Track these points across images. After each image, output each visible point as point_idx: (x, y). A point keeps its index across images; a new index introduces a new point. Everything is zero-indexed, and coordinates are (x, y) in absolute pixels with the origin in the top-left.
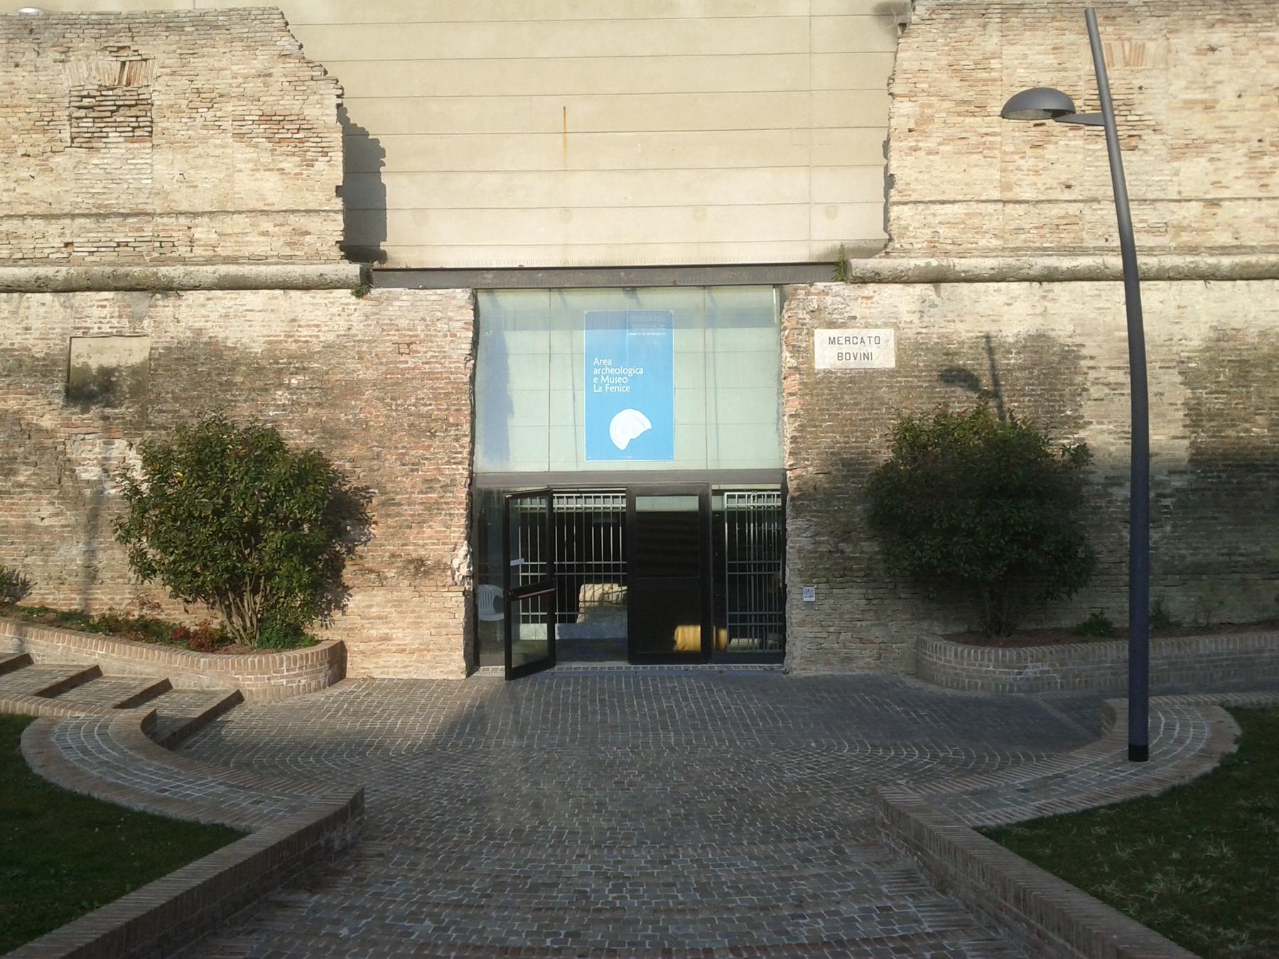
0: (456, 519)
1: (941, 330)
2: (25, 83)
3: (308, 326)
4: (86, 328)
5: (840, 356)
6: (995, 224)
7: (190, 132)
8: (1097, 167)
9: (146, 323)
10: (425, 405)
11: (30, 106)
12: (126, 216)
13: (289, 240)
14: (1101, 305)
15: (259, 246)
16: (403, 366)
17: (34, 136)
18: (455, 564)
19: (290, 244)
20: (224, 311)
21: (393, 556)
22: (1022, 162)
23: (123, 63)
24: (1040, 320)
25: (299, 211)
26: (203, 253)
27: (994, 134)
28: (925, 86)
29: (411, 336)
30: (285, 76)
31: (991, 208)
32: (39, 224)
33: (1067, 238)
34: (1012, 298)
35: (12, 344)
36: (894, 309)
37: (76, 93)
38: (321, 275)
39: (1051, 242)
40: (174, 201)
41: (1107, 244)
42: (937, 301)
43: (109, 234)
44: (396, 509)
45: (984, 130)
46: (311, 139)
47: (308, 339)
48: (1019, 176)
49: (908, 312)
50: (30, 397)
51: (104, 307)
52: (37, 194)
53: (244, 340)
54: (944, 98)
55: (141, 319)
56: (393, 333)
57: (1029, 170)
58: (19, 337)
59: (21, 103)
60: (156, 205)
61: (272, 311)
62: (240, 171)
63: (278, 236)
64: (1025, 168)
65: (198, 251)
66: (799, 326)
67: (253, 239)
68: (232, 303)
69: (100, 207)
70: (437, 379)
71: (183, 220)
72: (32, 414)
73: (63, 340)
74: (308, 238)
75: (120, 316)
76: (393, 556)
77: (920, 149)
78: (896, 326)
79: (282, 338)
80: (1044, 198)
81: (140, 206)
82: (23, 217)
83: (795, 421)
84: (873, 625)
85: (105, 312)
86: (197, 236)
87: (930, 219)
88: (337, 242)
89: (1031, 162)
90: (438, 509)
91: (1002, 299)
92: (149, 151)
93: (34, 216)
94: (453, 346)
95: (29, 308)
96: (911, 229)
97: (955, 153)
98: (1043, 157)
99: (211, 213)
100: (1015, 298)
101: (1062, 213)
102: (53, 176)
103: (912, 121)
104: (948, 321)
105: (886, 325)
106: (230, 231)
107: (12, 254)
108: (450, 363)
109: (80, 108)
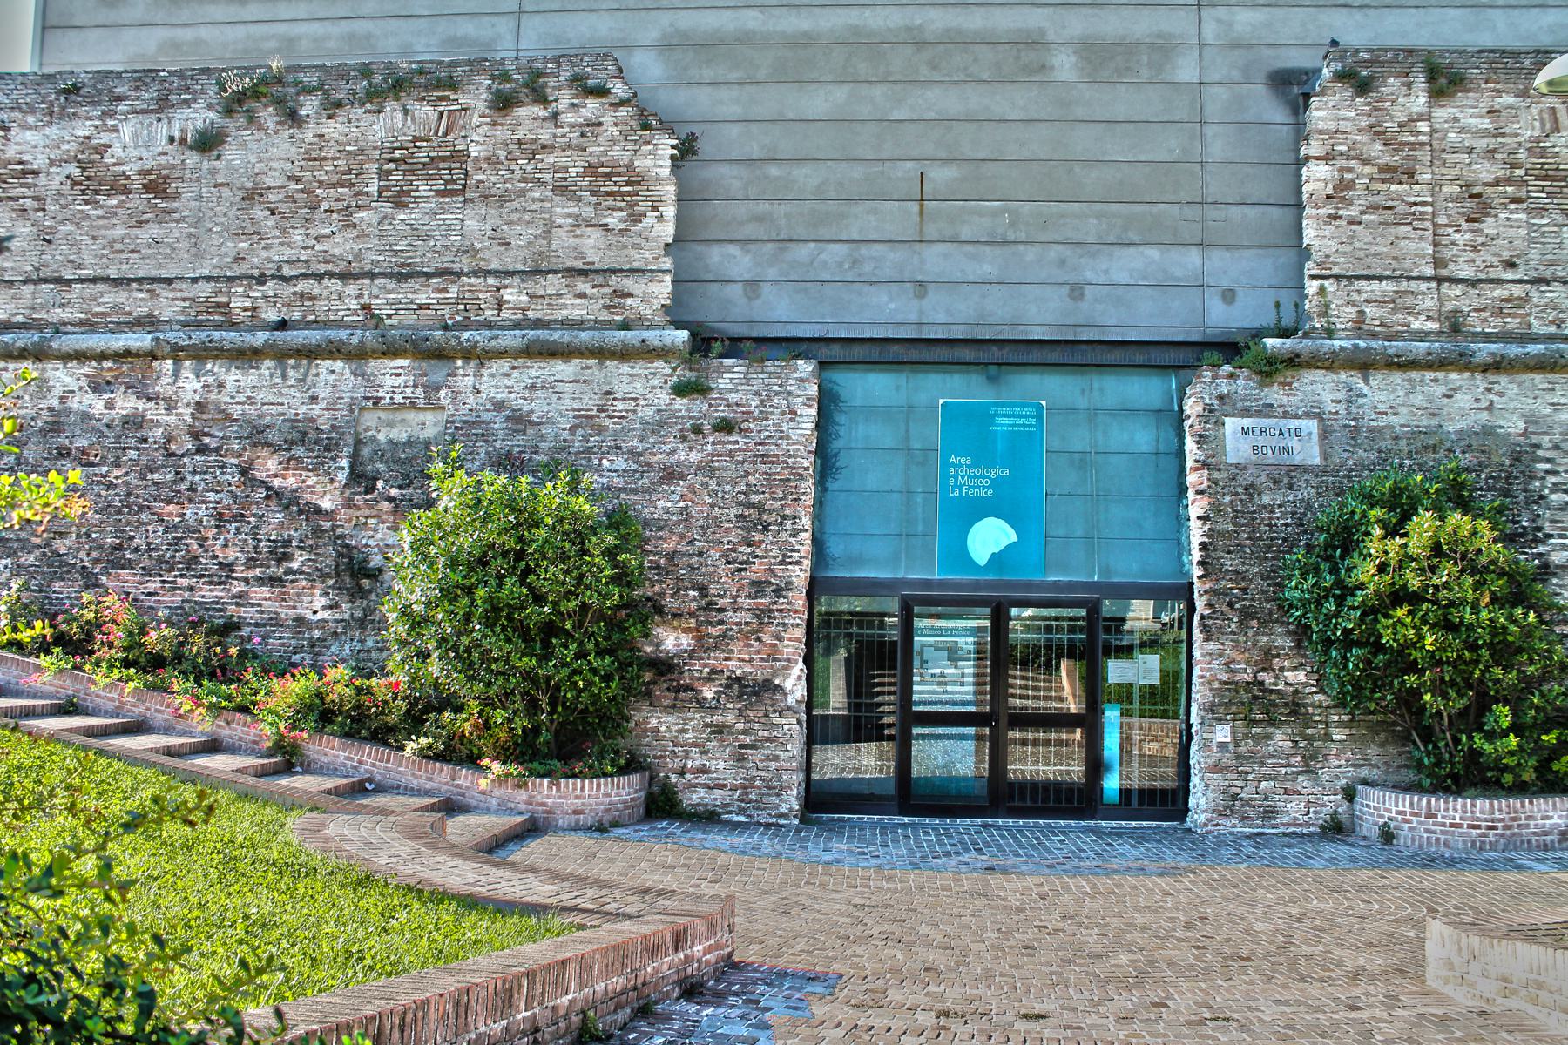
0: (790, 630)
1: (1372, 423)
2: (336, 135)
3: (624, 399)
4: (377, 398)
5: (1255, 449)
6: (1428, 304)
7: (507, 185)
8: (1544, 244)
9: (442, 393)
10: (757, 493)
11: (339, 158)
12: (429, 276)
14: (1555, 400)
15: (574, 309)
16: (731, 447)
17: (339, 190)
18: (788, 685)
21: (713, 671)
22: (1457, 236)
23: (441, 114)
24: (1485, 415)
25: (622, 271)
26: (513, 317)
27: (1424, 204)
28: (1344, 148)
29: (744, 413)
30: (616, 124)
31: (1423, 286)
32: (336, 284)
33: (1512, 323)
34: (1451, 389)
35: (297, 414)
36: (1317, 397)
37: (388, 145)
38: (643, 341)
39: (1494, 327)
40: (483, 259)
41: (1559, 332)
42: (1366, 390)
43: (410, 296)
44: (721, 616)
45: (1412, 199)
48: (1455, 252)
49: (1333, 401)
50: (310, 474)
51: (399, 375)
52: (337, 251)
53: (551, 414)
54: (1365, 162)
55: (438, 389)
57: (1465, 245)
58: (305, 407)
59: (330, 155)
60: (464, 264)
61: (585, 382)
62: (559, 226)
63: (597, 299)
64: (1461, 243)
65: (505, 314)
66: (1206, 413)
69: (403, 265)
70: (773, 463)
71: (491, 281)
72: (312, 493)
73: (352, 411)
74: (629, 301)
75: (415, 386)
76: (713, 671)
77: (1340, 217)
78: (1319, 417)
79: (594, 413)
80: (1483, 276)
81: (446, 265)
82: (319, 277)
83: (1205, 524)
84: (1301, 773)
85: (399, 381)
86: (506, 298)
87: (1355, 296)
88: (663, 306)
89: (1468, 236)
90: (769, 617)
91: (1439, 390)
92: (459, 205)
93: (331, 275)
94: (792, 425)
95: (317, 375)
96: (1333, 306)
97: (1380, 223)
98: (1481, 231)
99: (523, 272)
100: (1455, 390)
101: (1506, 294)
102: (355, 233)
103: (1330, 186)
104: (1380, 413)
105: (1307, 415)
106: (542, 293)
107: (304, 317)
108: (788, 444)
109: (391, 161)
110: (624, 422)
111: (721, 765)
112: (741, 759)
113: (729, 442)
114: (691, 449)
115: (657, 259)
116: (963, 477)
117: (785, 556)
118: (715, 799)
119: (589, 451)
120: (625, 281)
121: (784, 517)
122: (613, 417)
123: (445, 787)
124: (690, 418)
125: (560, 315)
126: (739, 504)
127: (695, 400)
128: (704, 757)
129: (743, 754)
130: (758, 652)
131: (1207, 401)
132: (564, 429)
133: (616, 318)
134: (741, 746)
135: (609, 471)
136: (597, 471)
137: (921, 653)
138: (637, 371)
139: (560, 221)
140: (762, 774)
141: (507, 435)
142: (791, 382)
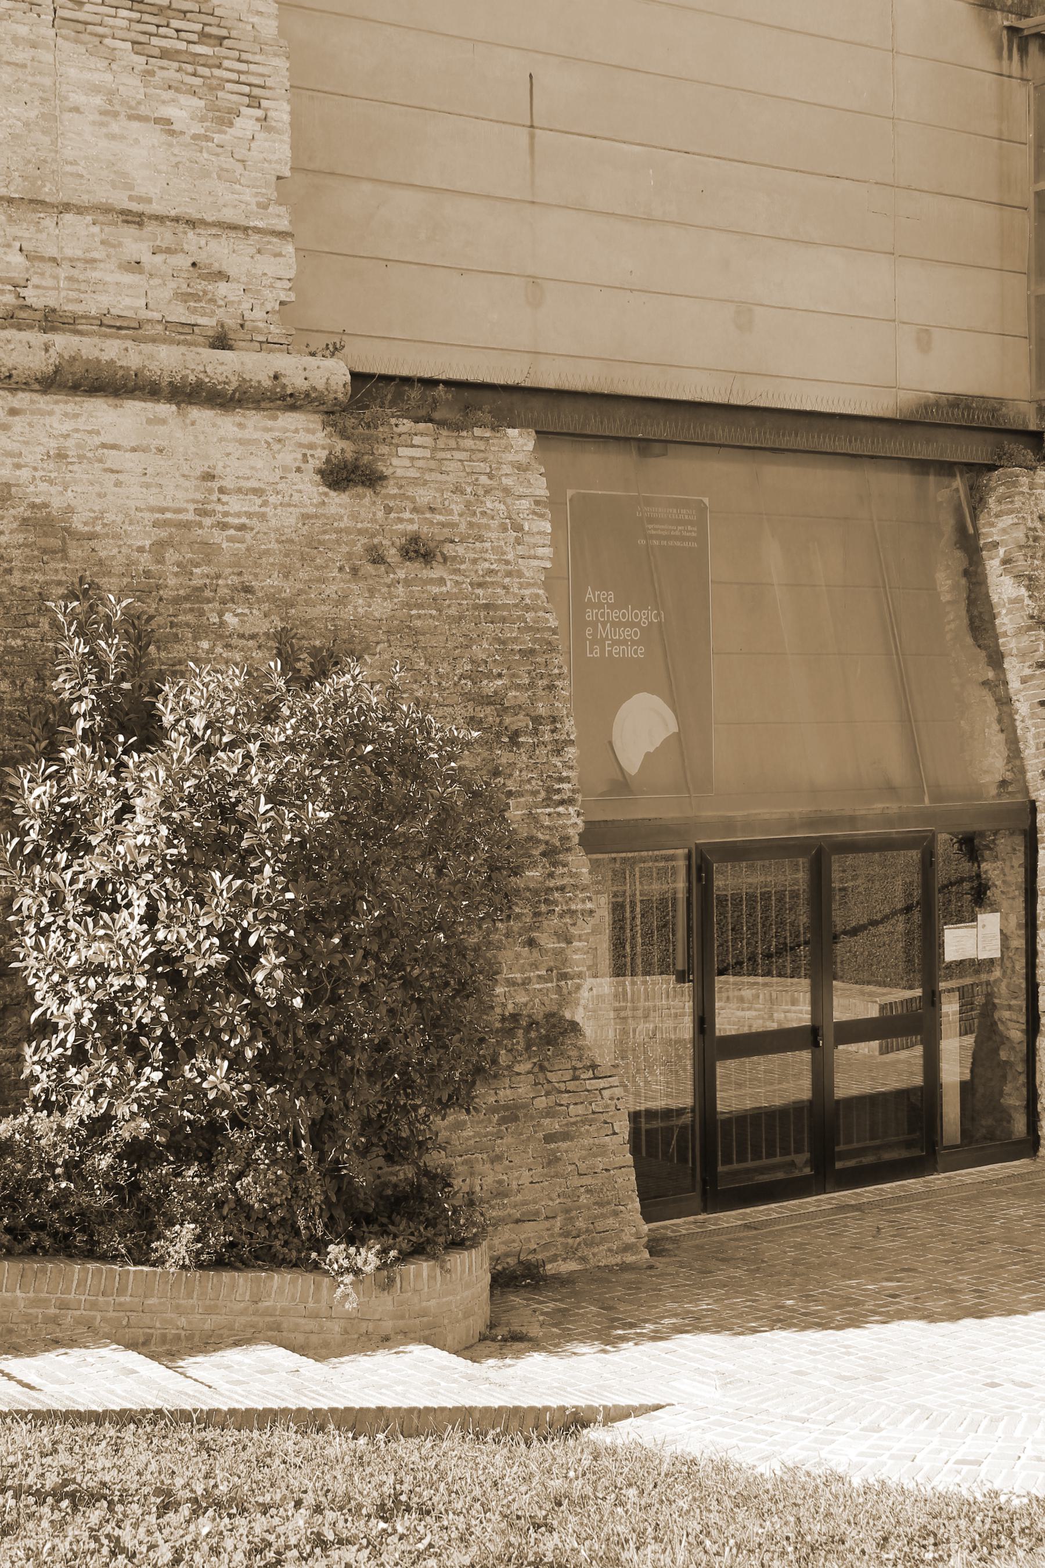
3: (239, 490)
10: (490, 676)
13: (184, 288)
16: (435, 590)
19: (185, 297)
20: (53, 444)
25: (204, 223)
29: (443, 525)
46: (226, 63)
47: (244, 520)
53: (109, 517)
56: (407, 515)
62: (76, 110)
67: (109, 278)
68: (67, 426)
70: (504, 620)
74: (222, 289)
94: (521, 550)
106: (52, 251)
108: (521, 586)
110: (248, 536)
111: (526, 1176)
112: (553, 1160)
113: (431, 581)
114: (372, 592)
115: (265, 207)
117: (550, 791)
118: (528, 1240)
119: (196, 595)
120: (213, 244)
121: (537, 720)
122: (224, 526)
123: (243, 1320)
124: (360, 532)
125: (93, 306)
126: (467, 697)
127: (361, 497)
128: (498, 1167)
129: (553, 1152)
130: (535, 966)
131: (1030, 524)
132: (141, 550)
133: (201, 321)
134: (549, 1138)
135: (242, 636)
136: (221, 637)
138: (249, 433)
139: (78, 98)
140: (586, 1180)
141: (30, 559)
142: (506, 469)
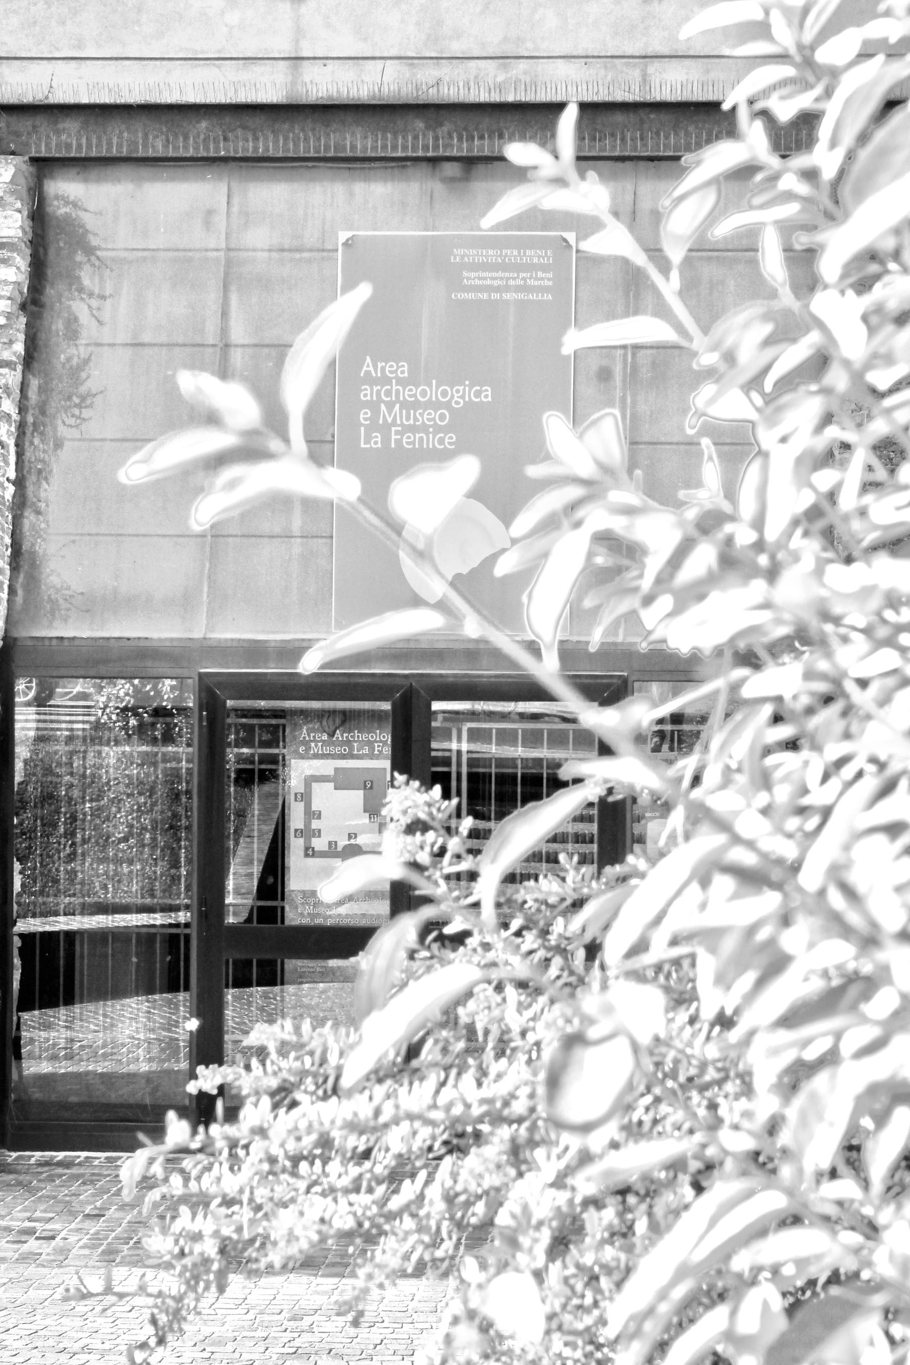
116: (390, 406)
137: (306, 797)
